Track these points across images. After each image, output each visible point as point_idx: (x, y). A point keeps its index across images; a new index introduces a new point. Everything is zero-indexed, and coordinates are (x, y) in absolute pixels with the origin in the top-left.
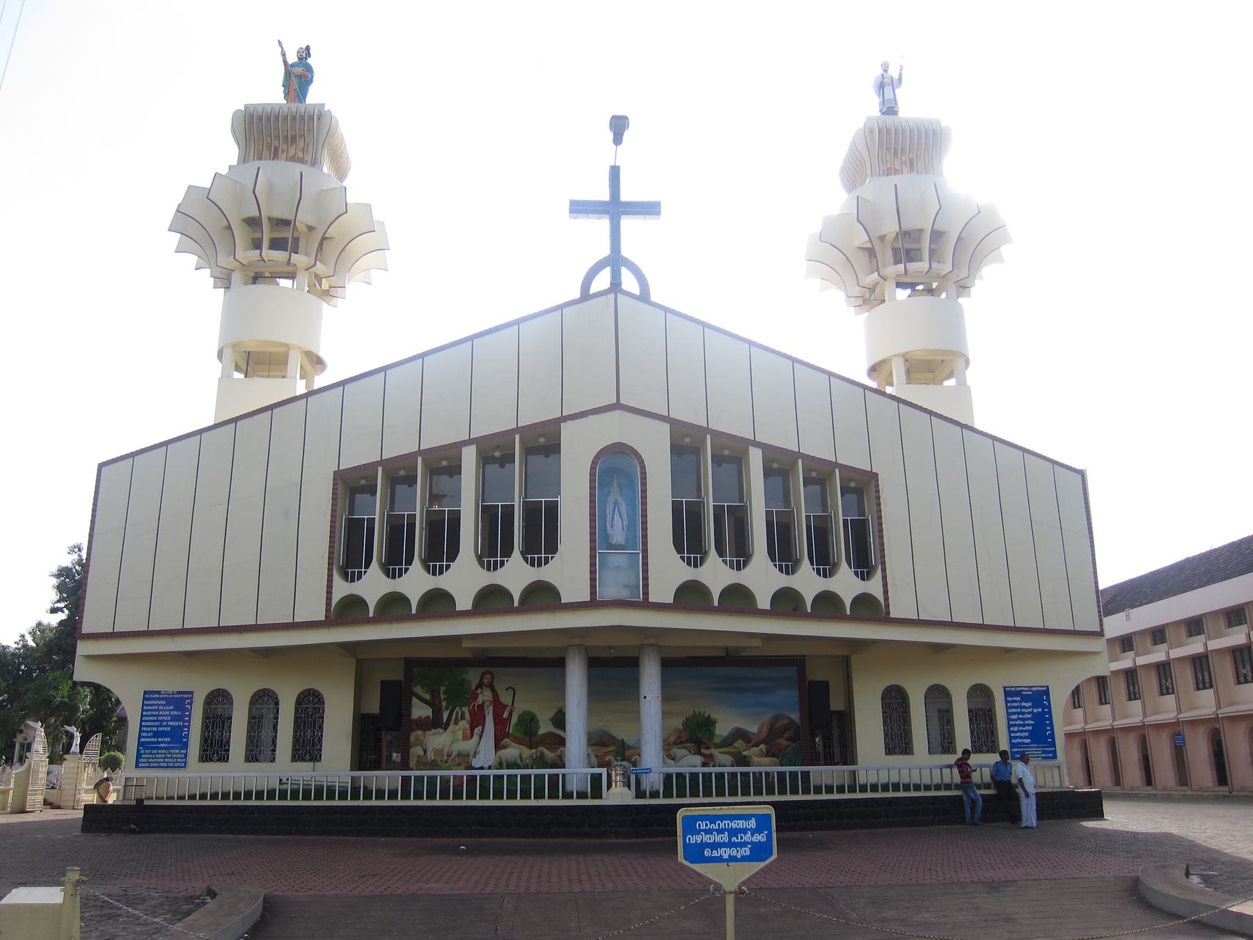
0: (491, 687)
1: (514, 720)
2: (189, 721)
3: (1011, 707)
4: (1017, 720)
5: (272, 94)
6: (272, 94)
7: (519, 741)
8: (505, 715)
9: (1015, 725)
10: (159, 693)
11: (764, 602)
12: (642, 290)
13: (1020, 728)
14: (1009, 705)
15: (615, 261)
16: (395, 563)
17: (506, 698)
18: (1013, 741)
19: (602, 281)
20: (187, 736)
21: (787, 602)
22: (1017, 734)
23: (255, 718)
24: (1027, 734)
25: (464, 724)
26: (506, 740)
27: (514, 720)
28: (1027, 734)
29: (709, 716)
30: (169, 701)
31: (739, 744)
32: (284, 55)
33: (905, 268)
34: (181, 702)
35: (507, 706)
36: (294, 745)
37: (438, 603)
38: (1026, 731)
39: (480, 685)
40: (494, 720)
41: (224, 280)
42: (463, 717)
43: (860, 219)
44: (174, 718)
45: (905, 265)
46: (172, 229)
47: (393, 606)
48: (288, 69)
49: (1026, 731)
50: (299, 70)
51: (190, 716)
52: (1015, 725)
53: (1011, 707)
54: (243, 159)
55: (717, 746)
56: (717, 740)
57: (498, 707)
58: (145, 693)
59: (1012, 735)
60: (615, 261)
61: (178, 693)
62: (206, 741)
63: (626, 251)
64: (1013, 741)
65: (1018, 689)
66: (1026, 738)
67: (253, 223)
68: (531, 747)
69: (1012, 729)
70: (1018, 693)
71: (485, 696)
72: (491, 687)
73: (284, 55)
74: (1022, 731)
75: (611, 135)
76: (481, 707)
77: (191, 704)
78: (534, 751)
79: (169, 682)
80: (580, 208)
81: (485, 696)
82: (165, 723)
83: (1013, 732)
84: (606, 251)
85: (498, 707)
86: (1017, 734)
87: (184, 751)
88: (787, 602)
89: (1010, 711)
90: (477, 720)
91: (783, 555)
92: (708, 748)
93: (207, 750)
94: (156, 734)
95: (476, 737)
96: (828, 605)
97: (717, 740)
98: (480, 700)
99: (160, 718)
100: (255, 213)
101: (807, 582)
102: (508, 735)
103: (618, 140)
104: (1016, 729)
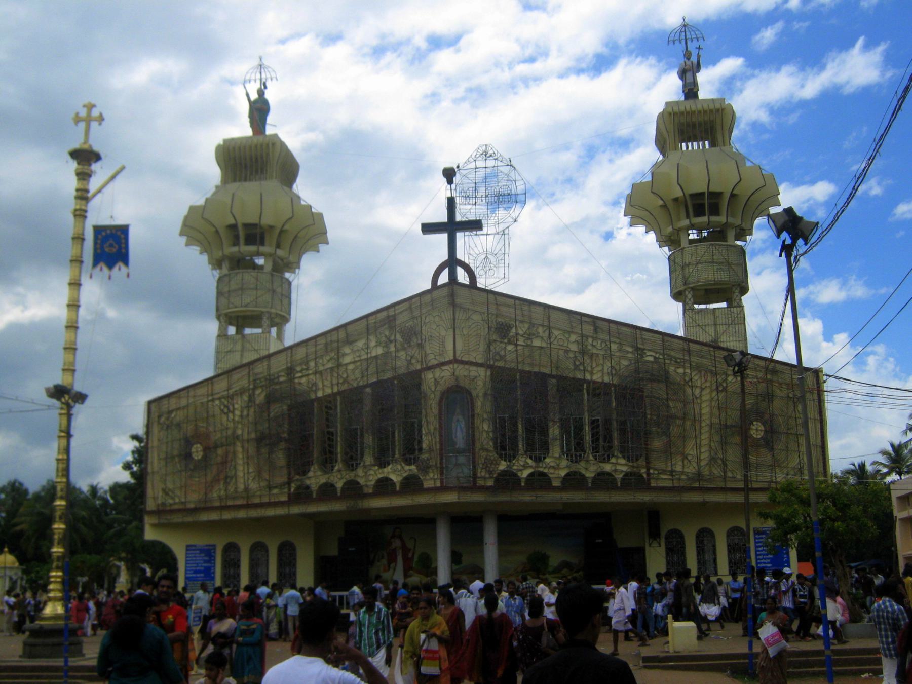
0: (400, 537)
1: (416, 558)
2: (214, 563)
3: (759, 542)
4: (762, 551)
5: (242, 129)
6: (242, 129)
7: (419, 572)
8: (410, 555)
9: (760, 555)
10: (195, 546)
11: (556, 483)
12: (471, 281)
13: (764, 557)
14: (757, 540)
15: (452, 262)
16: (327, 463)
17: (410, 544)
18: (759, 565)
19: (444, 278)
20: (214, 573)
21: (574, 481)
22: (762, 561)
23: (699, 547)
24: (769, 561)
25: (385, 561)
26: (411, 572)
27: (416, 558)
28: (769, 561)
29: (545, 553)
30: (201, 551)
31: (565, 571)
32: (248, 95)
33: (709, 220)
34: (209, 552)
35: (410, 550)
36: (729, 564)
37: (539, 481)
38: (768, 559)
39: (393, 536)
40: (403, 559)
41: (217, 263)
42: (383, 558)
43: (680, 182)
44: (205, 562)
45: (709, 218)
46: (181, 234)
47: (327, 492)
48: (253, 105)
49: (768, 559)
50: (259, 105)
51: (214, 560)
52: (760, 555)
53: (759, 542)
54: (225, 180)
55: (550, 573)
56: (550, 569)
57: (405, 550)
58: (188, 546)
59: (759, 561)
60: (452, 262)
61: (207, 546)
62: (281, 575)
63: (460, 255)
64: (759, 565)
65: (764, 529)
66: (768, 563)
67: (233, 227)
68: (427, 576)
69: (758, 557)
70: (763, 533)
71: (397, 543)
72: (400, 537)
73: (248, 95)
74: (765, 559)
75: (445, 180)
76: (394, 550)
77: (214, 552)
78: (429, 578)
79: (201, 541)
80: (428, 228)
81: (397, 543)
82: (200, 565)
83: (760, 559)
84: (444, 256)
85: (405, 550)
86: (762, 561)
87: (212, 582)
88: (508, 481)
89: (757, 545)
90: (392, 559)
91: (575, 450)
92: (544, 574)
93: (732, 567)
94: (196, 572)
95: (391, 571)
96: (604, 481)
97: (550, 569)
98: (394, 546)
99: (197, 562)
100: (232, 222)
101: (589, 469)
102: (411, 568)
103: (450, 182)
104: (761, 557)
